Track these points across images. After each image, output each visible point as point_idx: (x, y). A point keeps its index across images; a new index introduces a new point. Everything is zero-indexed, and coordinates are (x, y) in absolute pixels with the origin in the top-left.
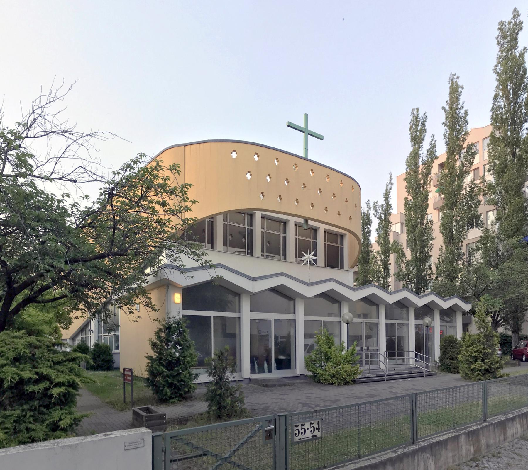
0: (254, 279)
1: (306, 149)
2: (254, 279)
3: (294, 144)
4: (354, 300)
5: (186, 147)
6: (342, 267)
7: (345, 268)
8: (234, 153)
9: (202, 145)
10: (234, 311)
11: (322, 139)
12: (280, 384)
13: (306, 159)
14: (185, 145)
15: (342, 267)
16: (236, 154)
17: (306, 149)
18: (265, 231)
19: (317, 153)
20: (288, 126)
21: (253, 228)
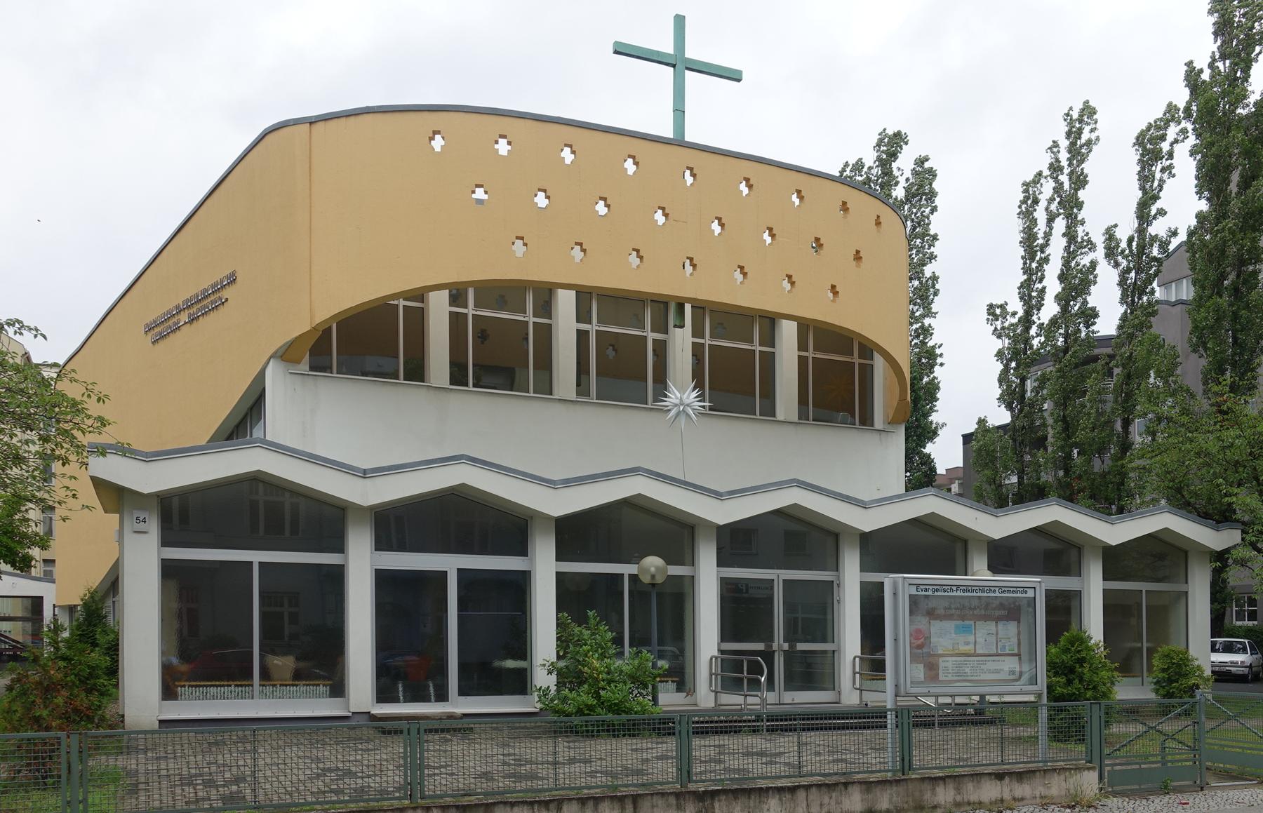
0: (364, 474)
1: (679, 112)
2: (364, 474)
3: (641, 102)
4: (146, 490)
5: (315, 127)
6: (866, 420)
7: (780, 415)
8: (503, 142)
9: (352, 119)
10: (682, 564)
11: (739, 80)
12: (782, 723)
13: (678, 142)
14: (312, 121)
15: (866, 420)
16: (509, 143)
17: (679, 112)
18: (811, 354)
19: (716, 118)
20: (616, 52)
21: (777, 350)
